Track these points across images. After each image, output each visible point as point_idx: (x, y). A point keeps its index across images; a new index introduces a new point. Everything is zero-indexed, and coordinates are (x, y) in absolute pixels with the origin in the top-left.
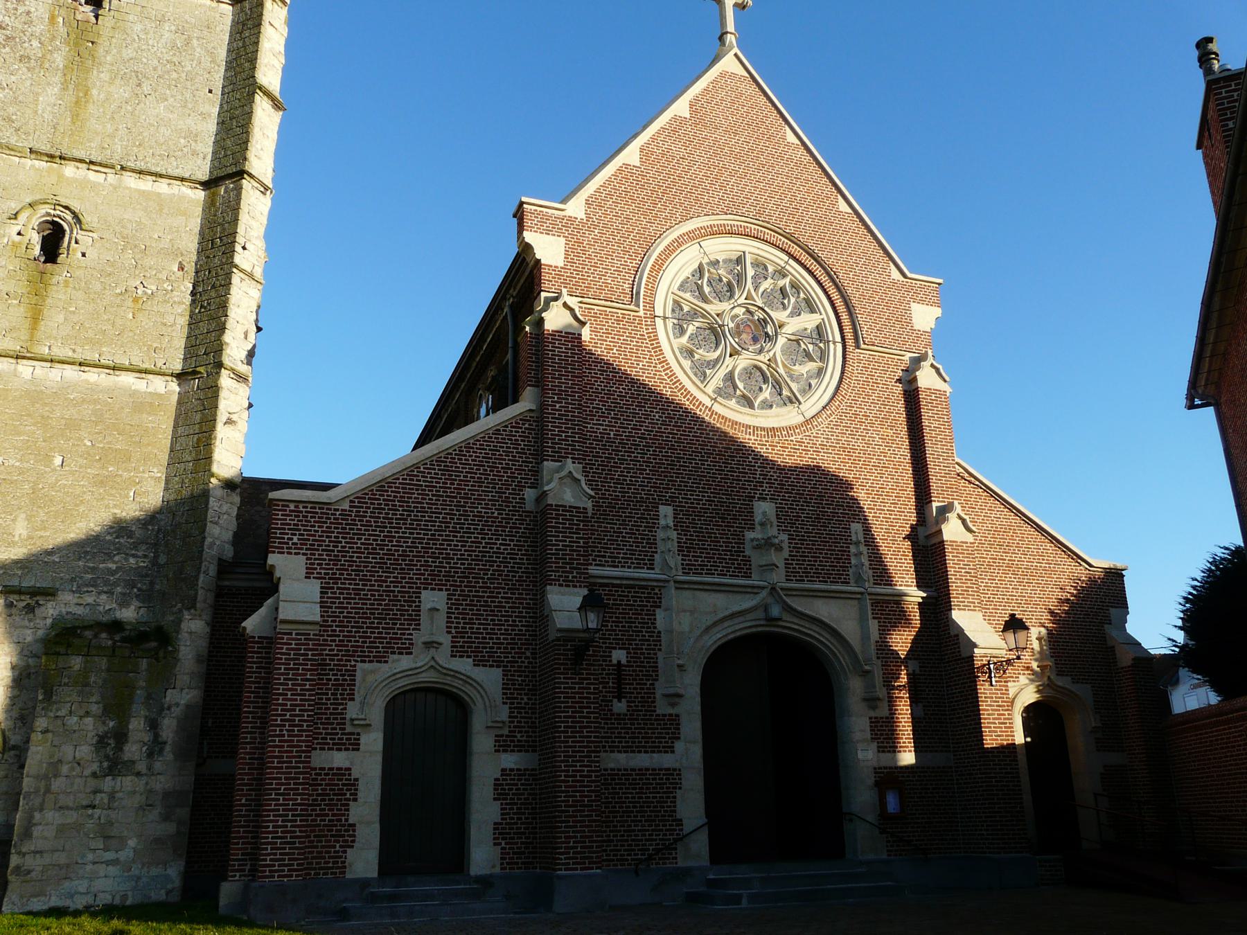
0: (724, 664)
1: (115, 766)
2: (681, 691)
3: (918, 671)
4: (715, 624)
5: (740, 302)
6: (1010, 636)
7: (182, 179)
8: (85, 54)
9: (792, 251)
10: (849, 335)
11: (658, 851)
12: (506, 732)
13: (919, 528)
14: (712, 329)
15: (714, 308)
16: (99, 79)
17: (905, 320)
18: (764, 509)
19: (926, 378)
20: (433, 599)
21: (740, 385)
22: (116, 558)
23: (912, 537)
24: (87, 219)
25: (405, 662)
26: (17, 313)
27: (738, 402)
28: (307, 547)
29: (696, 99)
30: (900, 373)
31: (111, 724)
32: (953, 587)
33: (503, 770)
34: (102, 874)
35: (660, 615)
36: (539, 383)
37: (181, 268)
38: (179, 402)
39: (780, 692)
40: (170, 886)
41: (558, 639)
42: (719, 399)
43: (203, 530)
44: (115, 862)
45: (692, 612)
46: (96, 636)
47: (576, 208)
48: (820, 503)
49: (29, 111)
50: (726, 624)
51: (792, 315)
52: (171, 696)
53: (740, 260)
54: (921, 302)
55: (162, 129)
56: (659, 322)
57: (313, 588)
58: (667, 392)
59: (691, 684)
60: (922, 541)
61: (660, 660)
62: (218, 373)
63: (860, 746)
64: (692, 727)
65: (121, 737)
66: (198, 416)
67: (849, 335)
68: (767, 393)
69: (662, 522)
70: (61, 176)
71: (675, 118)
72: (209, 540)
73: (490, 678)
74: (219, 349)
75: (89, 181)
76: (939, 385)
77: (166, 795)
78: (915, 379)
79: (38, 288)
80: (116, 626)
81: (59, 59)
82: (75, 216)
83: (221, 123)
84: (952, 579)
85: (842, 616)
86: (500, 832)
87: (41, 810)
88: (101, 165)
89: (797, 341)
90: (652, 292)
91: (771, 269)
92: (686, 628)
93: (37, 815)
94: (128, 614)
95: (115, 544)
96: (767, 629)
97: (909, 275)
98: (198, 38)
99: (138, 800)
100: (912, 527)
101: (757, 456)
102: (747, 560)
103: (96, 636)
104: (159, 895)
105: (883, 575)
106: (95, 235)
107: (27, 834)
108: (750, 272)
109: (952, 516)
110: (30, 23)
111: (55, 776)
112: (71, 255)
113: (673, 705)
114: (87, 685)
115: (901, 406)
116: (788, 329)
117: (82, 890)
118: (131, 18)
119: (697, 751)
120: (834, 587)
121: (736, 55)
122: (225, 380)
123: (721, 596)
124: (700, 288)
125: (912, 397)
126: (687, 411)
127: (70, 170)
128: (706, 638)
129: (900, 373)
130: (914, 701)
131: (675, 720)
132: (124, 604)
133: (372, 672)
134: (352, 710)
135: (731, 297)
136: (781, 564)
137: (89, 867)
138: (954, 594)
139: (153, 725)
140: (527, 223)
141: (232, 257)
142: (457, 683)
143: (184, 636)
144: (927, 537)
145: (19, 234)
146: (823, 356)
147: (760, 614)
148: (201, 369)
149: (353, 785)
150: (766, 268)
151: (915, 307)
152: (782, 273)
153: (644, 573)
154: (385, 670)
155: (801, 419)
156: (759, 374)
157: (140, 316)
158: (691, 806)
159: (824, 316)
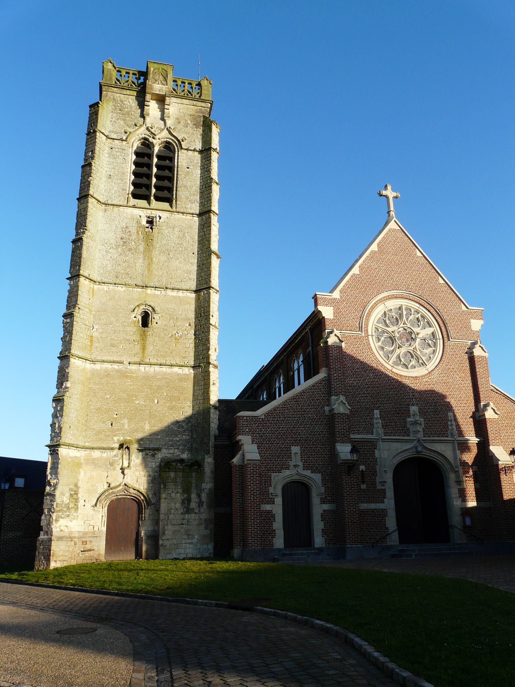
0: (401, 469)
1: (188, 510)
2: (386, 480)
3: (477, 470)
4: (397, 455)
5: (401, 326)
6: (512, 456)
7: (187, 290)
8: (150, 245)
9: (421, 302)
10: (445, 336)
11: (380, 539)
12: (324, 496)
13: (476, 413)
14: (390, 338)
15: (390, 330)
16: (155, 252)
17: (468, 327)
18: (414, 409)
19: (477, 352)
20: (295, 449)
21: (402, 360)
22: (179, 436)
23: (473, 417)
24: (156, 309)
25: (287, 473)
26: (138, 348)
27: (402, 367)
28: (251, 432)
29: (380, 242)
30: (467, 350)
31: (186, 496)
32: (490, 436)
33: (324, 510)
34: (188, 547)
35: (376, 452)
36: (327, 366)
37: (190, 325)
38: (194, 377)
39: (424, 480)
40: (210, 552)
41: (342, 463)
42: (395, 366)
43: (209, 425)
44: (192, 543)
45: (388, 450)
46: (176, 464)
47: (336, 294)
48: (435, 405)
49: (134, 270)
50: (401, 454)
51: (421, 329)
52: (204, 486)
53: (400, 308)
54: (475, 318)
55: (178, 271)
56: (370, 337)
57: (255, 447)
58: (375, 365)
59: (389, 478)
60: (477, 418)
61: (377, 469)
62: (209, 366)
63: (455, 500)
64: (390, 494)
65: (189, 500)
66: (203, 383)
67: (445, 336)
68: (413, 362)
69: (375, 416)
70: (146, 294)
71: (372, 252)
72: (211, 429)
73: (317, 477)
74: (208, 357)
75: (156, 294)
76: (483, 354)
77: (206, 520)
78: (473, 352)
79: (144, 337)
80: (182, 461)
81: (141, 248)
82: (153, 309)
83: (198, 266)
84: (489, 433)
85: (445, 449)
86: (324, 532)
87: (167, 525)
88: (159, 288)
89: (424, 340)
90: (367, 325)
91: (413, 311)
92: (386, 456)
93: (166, 527)
94: (185, 456)
95: (178, 431)
96: (417, 456)
97: (469, 308)
98: (187, 233)
99: (196, 522)
100: (473, 413)
101: (410, 388)
102: (408, 429)
103: (176, 464)
104: (206, 555)
105: (461, 433)
106: (159, 315)
107: (164, 534)
108: (405, 313)
109: (489, 409)
110: (130, 235)
111: (170, 514)
112: (152, 325)
113: (383, 485)
114: (176, 482)
115: (467, 363)
116: (420, 336)
117: (182, 552)
118: (164, 228)
119: (392, 502)
120: (442, 439)
121: (395, 221)
122: (211, 369)
123: (399, 443)
124: (385, 321)
125: (472, 360)
126: (382, 373)
127: (149, 291)
128: (394, 460)
129: (467, 350)
130: (476, 481)
131: (384, 491)
132: (183, 453)
133: (277, 476)
134: (271, 490)
135: (397, 324)
136: (421, 430)
137: (184, 545)
138: (490, 439)
139: (199, 496)
140: (319, 302)
141: (209, 321)
142: (306, 480)
143: (206, 464)
144: (480, 416)
145: (135, 317)
146: (435, 345)
147: (414, 450)
148: (202, 365)
149: (273, 516)
150: (411, 311)
151: (472, 321)
152: (417, 312)
153: (370, 436)
154: (281, 475)
155: (427, 372)
156: (411, 355)
157: (177, 344)
158: (391, 522)
159: (435, 328)
